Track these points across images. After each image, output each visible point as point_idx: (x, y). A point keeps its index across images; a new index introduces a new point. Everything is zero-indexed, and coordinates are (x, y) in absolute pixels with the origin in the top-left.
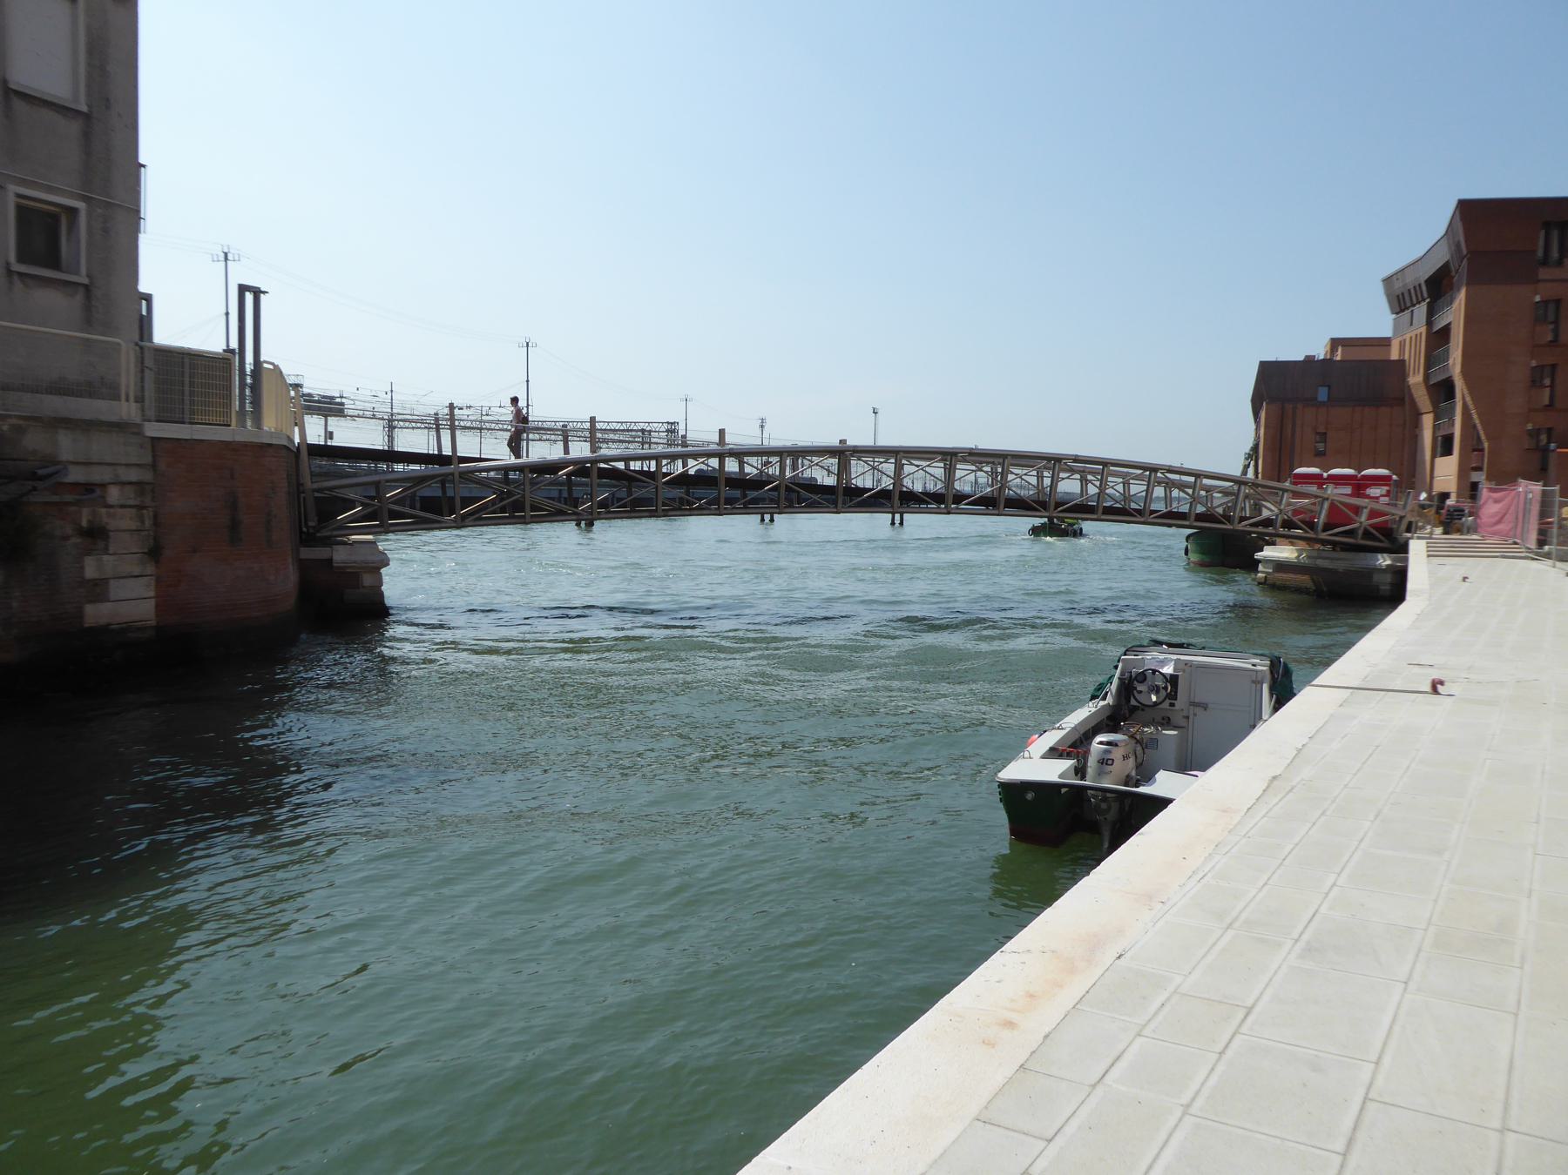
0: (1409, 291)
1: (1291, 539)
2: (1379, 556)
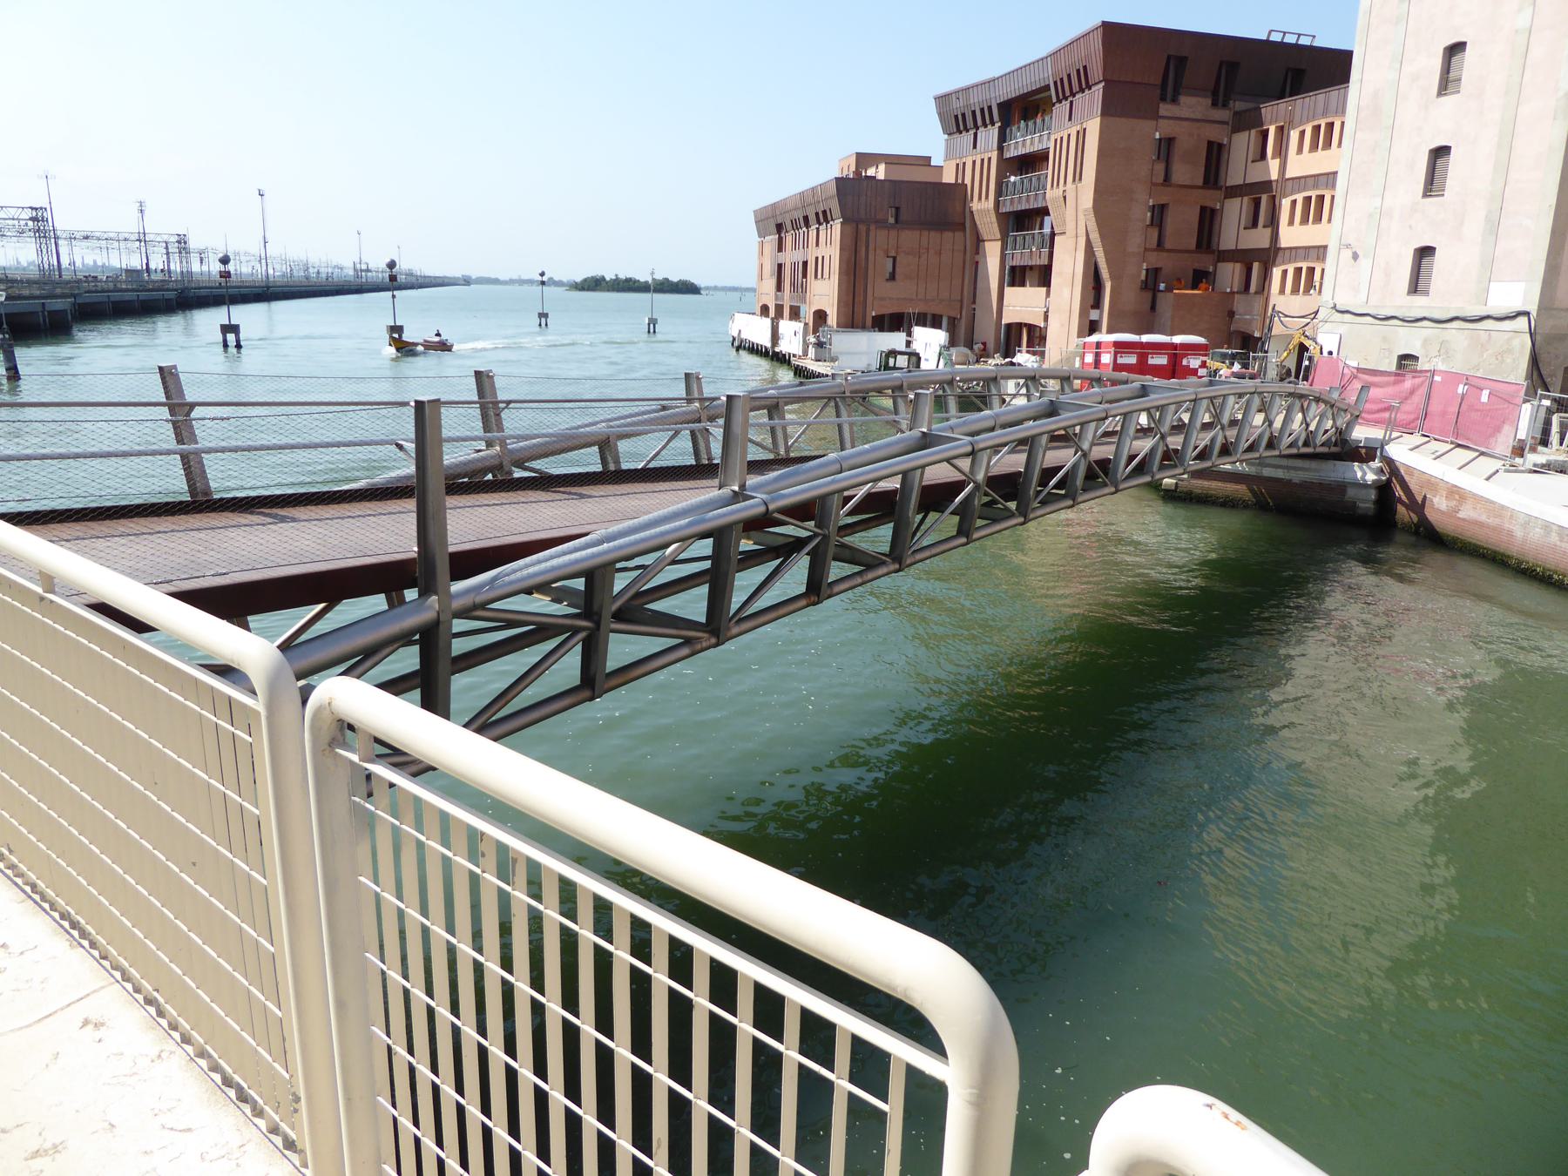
0: (974, 113)
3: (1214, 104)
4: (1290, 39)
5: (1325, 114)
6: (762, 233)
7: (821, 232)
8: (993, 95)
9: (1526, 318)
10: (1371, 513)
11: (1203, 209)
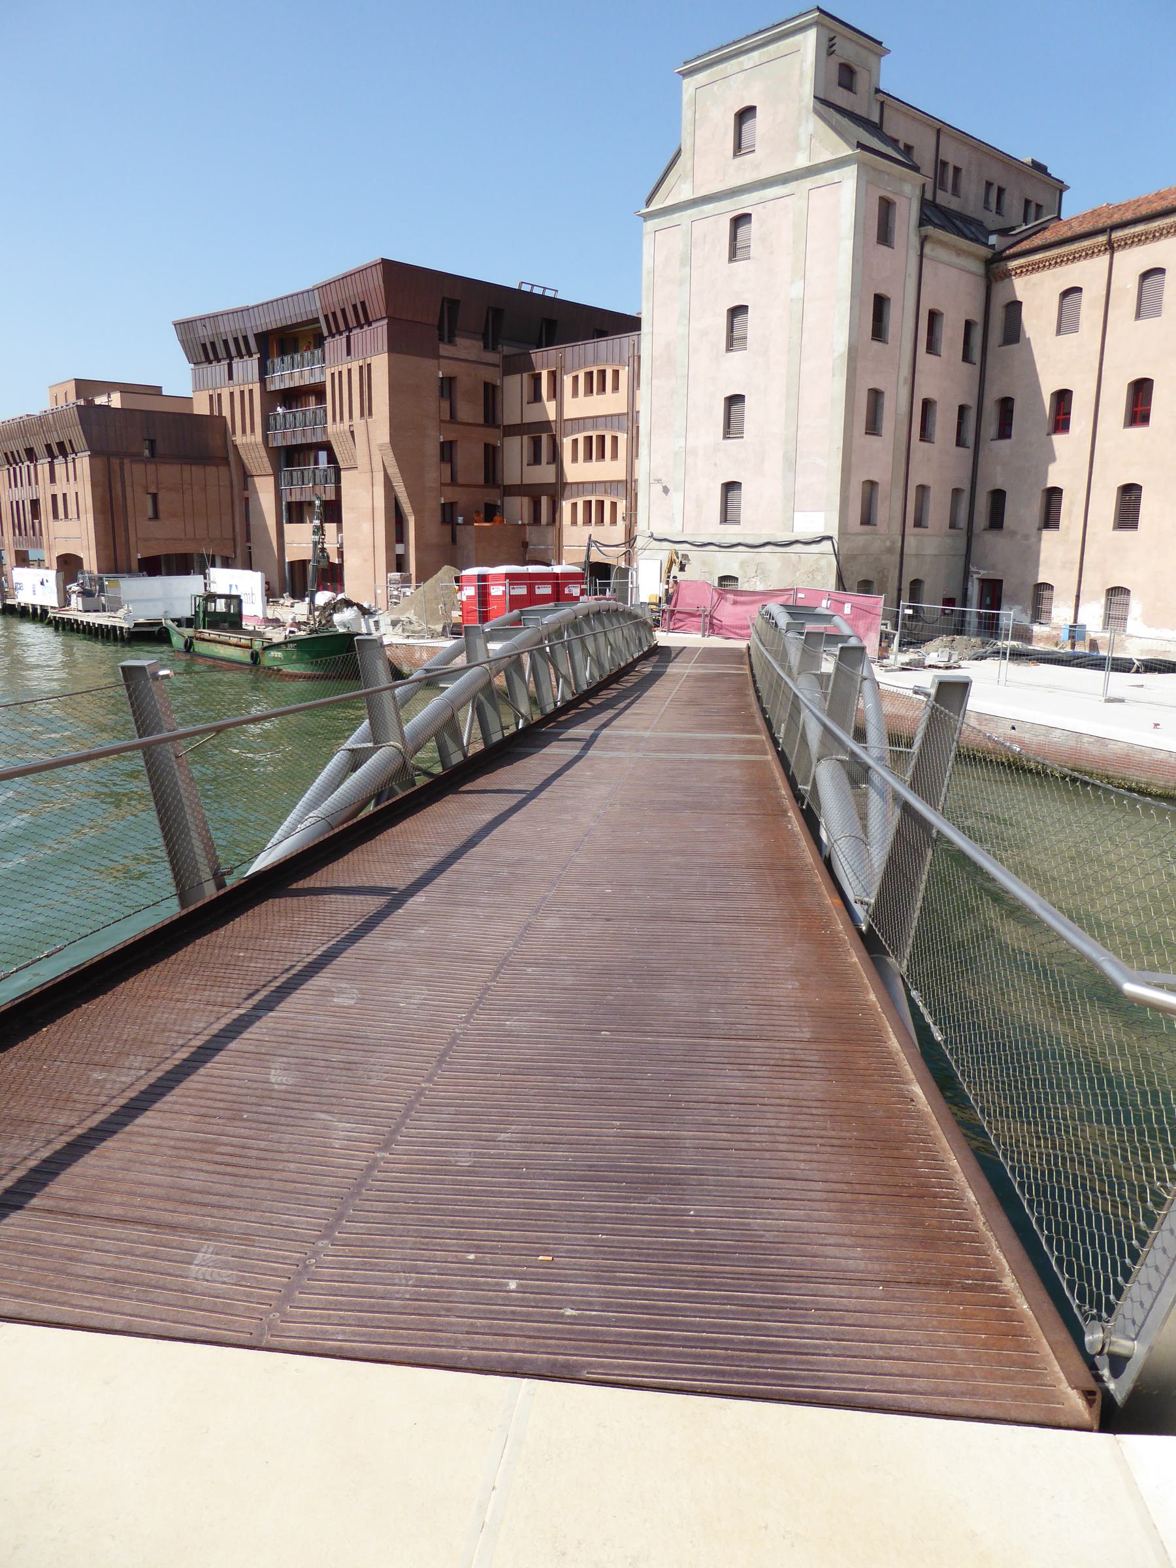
0: (226, 342)
3: (486, 347)
4: (538, 291)
5: (595, 363)
9: (830, 542)
11: (486, 446)
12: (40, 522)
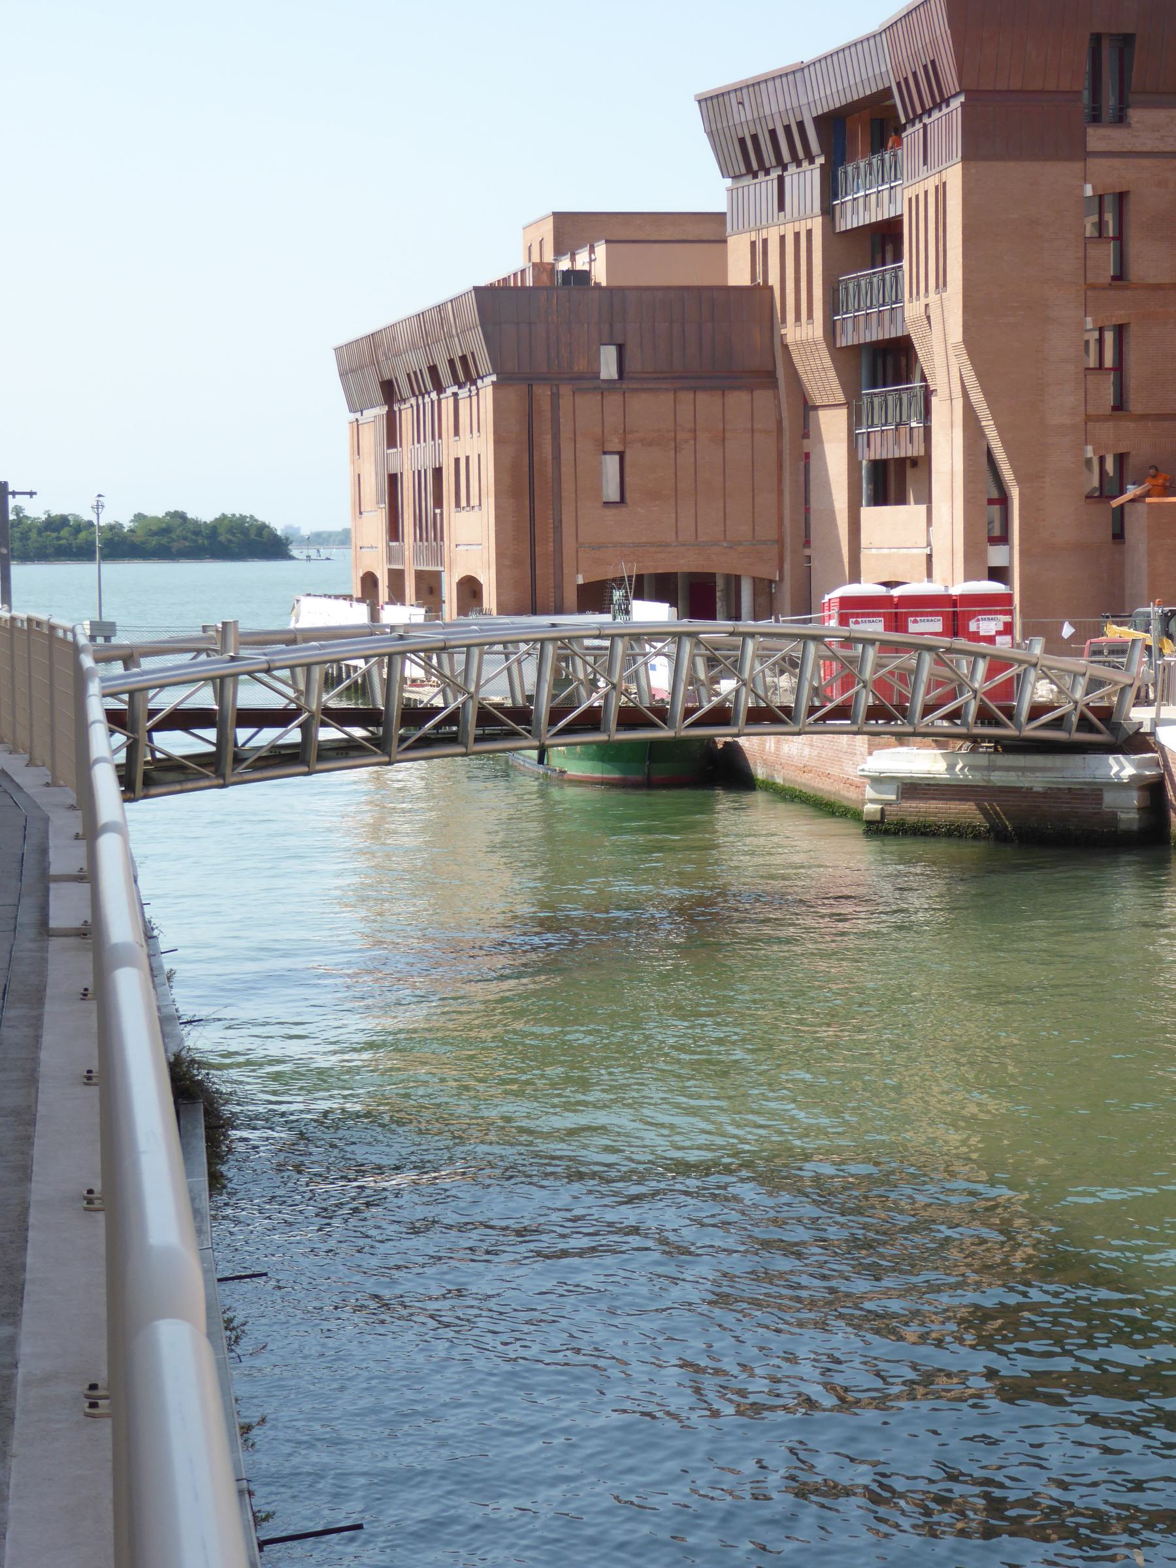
0: (773, 133)
1: (940, 739)
2: (1111, 759)
6: (356, 405)
7: (461, 403)
8: (803, 101)
10: (1135, 827)
12: (442, 514)
